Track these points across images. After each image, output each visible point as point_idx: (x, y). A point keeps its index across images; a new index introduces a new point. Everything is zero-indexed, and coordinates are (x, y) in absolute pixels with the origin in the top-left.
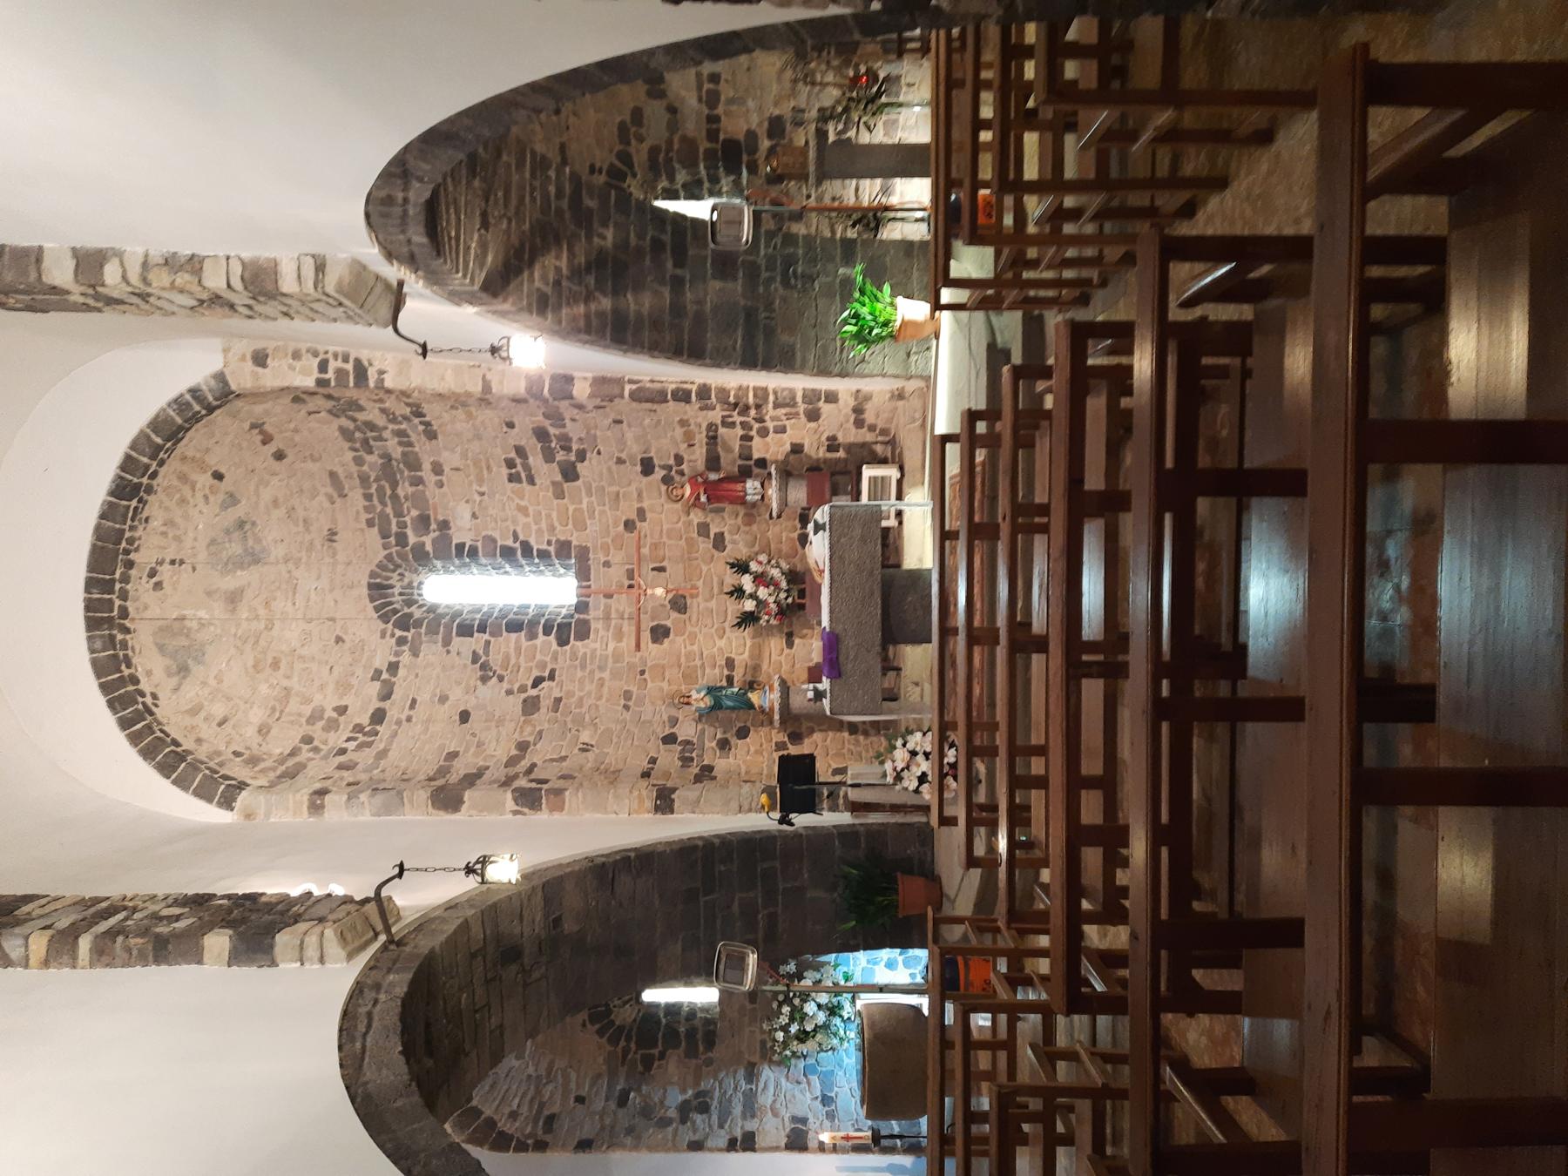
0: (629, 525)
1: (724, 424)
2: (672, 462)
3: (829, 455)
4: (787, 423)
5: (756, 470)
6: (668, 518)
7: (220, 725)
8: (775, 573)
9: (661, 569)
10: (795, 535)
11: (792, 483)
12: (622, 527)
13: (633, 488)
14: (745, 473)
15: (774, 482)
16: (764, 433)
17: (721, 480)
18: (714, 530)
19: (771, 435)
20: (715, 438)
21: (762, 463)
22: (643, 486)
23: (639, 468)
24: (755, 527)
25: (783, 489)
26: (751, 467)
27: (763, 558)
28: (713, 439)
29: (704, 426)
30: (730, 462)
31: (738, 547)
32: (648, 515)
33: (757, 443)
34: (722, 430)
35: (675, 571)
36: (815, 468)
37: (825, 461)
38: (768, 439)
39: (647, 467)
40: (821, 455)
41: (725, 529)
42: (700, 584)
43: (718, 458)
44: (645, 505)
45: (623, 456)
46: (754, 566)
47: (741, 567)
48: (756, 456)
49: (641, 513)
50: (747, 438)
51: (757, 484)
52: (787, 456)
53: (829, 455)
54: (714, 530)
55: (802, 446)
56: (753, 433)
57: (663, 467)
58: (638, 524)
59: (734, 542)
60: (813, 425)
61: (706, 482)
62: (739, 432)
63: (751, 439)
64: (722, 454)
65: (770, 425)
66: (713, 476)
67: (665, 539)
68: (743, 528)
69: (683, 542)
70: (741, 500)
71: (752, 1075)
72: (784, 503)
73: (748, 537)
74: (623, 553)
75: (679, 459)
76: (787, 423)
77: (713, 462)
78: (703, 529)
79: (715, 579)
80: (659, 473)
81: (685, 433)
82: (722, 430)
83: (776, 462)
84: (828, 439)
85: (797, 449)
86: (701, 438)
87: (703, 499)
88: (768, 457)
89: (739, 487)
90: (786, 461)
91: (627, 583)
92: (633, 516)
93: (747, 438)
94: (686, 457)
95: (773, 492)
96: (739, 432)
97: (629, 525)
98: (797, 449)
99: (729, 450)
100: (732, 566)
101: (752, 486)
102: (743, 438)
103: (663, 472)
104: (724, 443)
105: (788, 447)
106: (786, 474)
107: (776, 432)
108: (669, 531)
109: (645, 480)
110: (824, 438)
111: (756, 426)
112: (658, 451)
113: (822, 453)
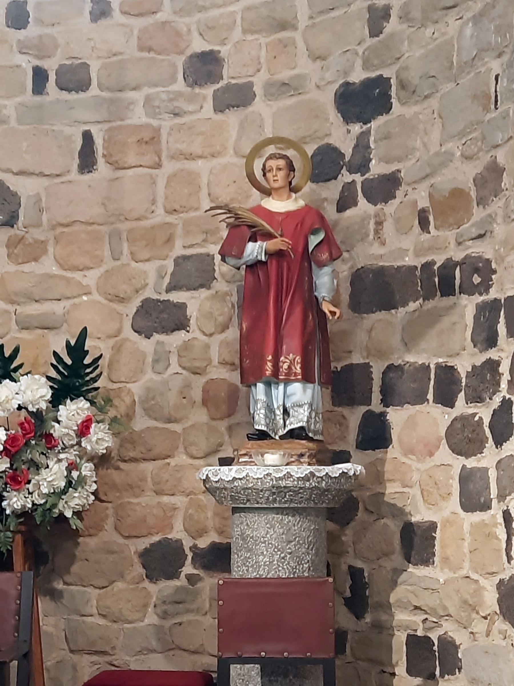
0: (205, 67)
1: (488, 313)
2: (377, 168)
3: (400, 639)
4: (496, 511)
5: (354, 417)
6: (214, 168)
7: (488, 635)
8: (52, 475)
9: (87, 160)
10: (177, 532)
11: (301, 528)
12: (199, 45)
13: (305, 66)
14: (343, 386)
15: (300, 471)
16: (464, 439)
17: (313, 304)
18: (194, 302)
19: (458, 462)
20: (447, 288)
21: (375, 435)
22: (313, 95)
23: (358, 76)
24: (200, 416)
25: (281, 500)
26: (359, 401)
27: (100, 439)
28: (442, 281)
29: (484, 249)
30: (375, 340)
31: (141, 370)
32: (232, 118)
33: (435, 418)
34: (468, 306)
35: (83, 195)
36: (359, 596)
37: (383, 629)
38: (444, 454)
39: (363, 101)
40: (401, 616)
41: (194, 333)
42: (48, 265)
43: (389, 304)
44: (259, 105)
45: (392, 26)
46: (73, 411)
47: (73, 377)
48: (396, 416)
49: (236, 98)
50: (447, 385)
51: (299, 418)
52: (397, 512)
53: (400, 639)
54: (194, 302)
55: (427, 560)
56: (462, 406)
57: (362, 145)
58: (208, 91)
59: (161, 359)
60: (491, 599)
61: (308, 260)
62: (466, 362)
63: (446, 399)
64: (401, 313)
65: (488, 459)
66: (325, 282)
67: (169, 167)
68: (199, 382)
69: (160, 216)
70: (251, 367)
71: (262, 456)
72: (238, 502)
73: (173, 398)
74: (132, 50)
75: (384, 189)
76: (496, 511)
77: (376, 290)
78: (193, 273)
79: (58, 308)
80: (343, 137)
81: (458, 194)
82: (468, 306)
83: (376, 474)
84: (449, 646)
85: (417, 542)
86: (446, 246)
87: (254, 250)
88: (393, 452)
89: (291, 360)
90: (379, 507)
91: (51, 66)
92: (231, 74)
93: (447, 385)
94: (391, 208)
95: (270, 466)
96: (466, 362)
97: (205, 67)
98: (417, 542)
99: (411, 338)
100: (77, 350)
101: (298, 400)
102: (447, 377)
103: (347, 150)
104: (432, 319)
105: (420, 515)
106: (340, 511)
107: (466, 477)
108: (191, 179)
109: (327, 98)
110: (449, 628)
111: (484, 413)
112: (408, 126)
113: (405, 621)
